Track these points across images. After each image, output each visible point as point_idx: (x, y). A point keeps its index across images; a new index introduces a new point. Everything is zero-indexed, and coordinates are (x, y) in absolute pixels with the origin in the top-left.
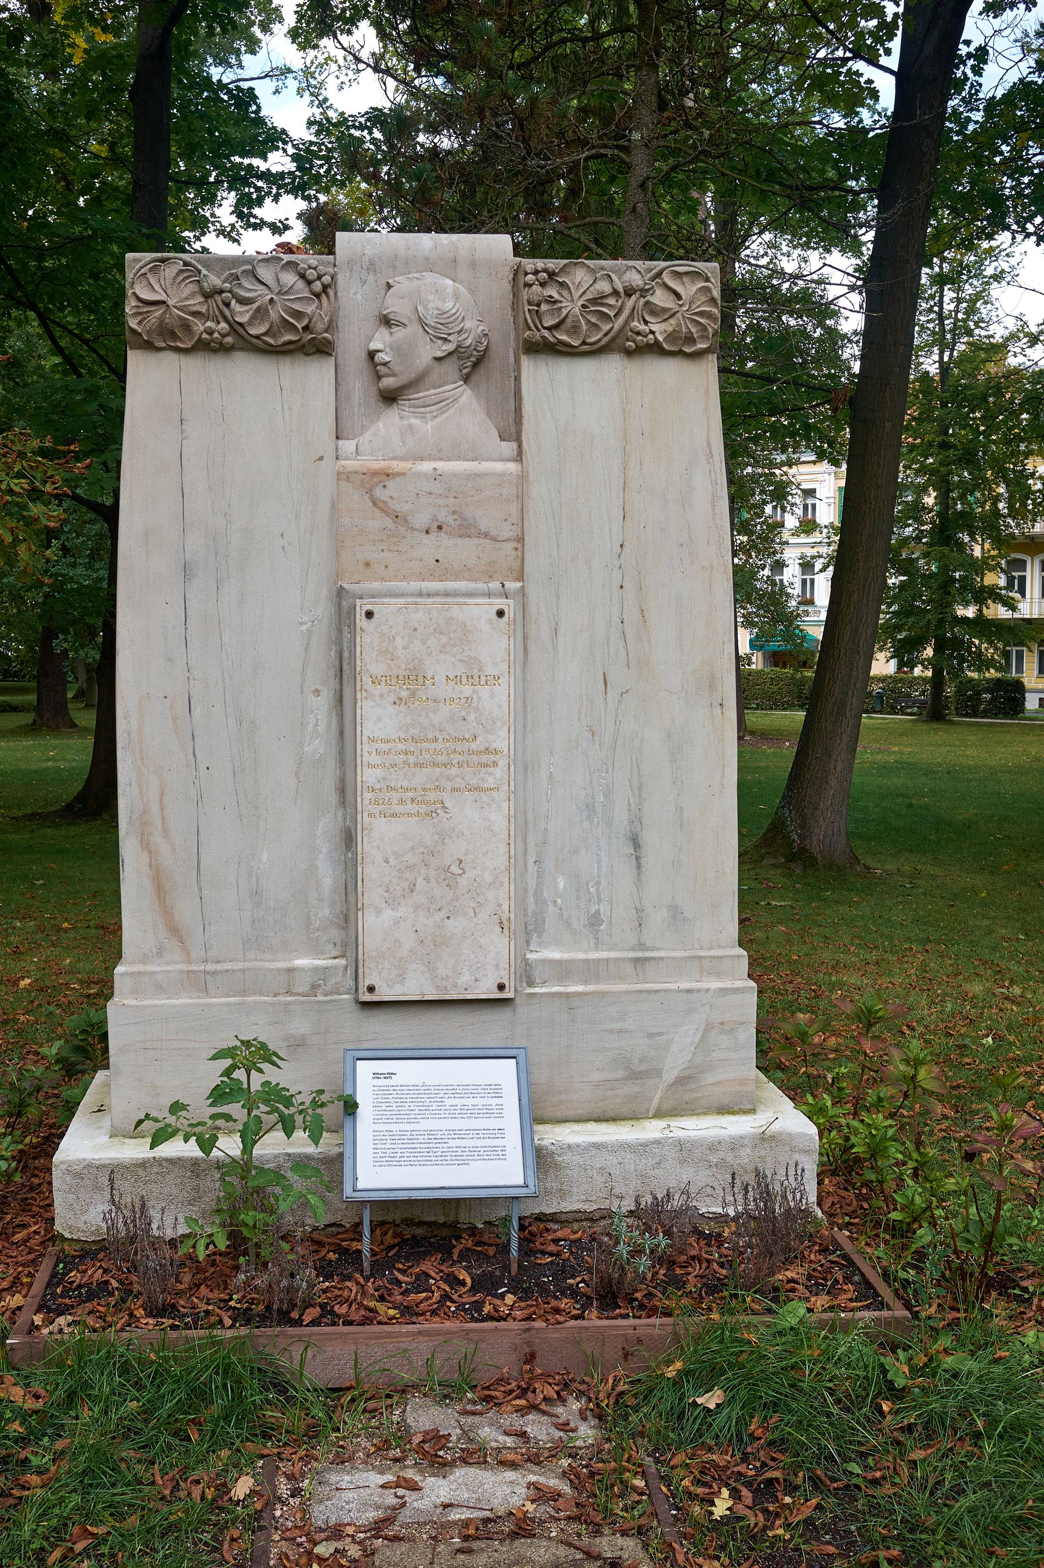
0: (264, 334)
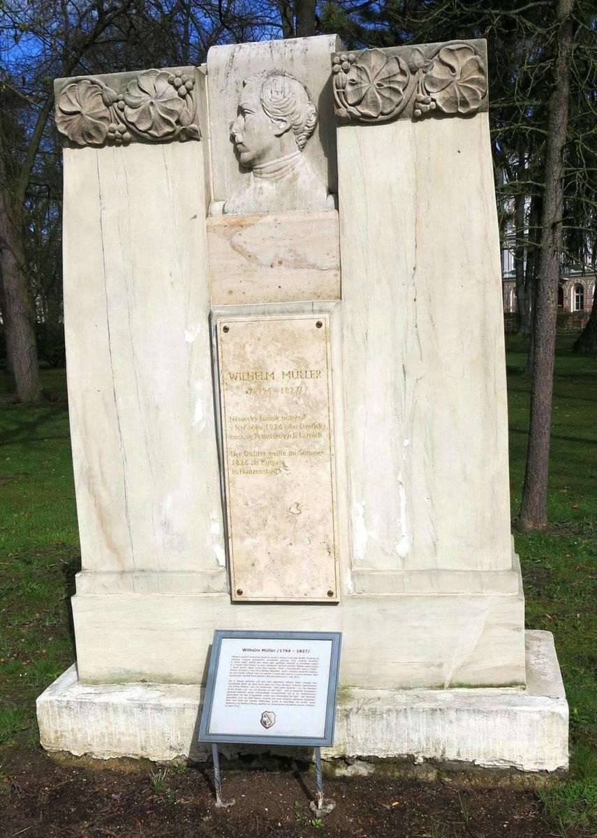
0: (150, 129)
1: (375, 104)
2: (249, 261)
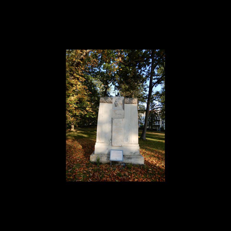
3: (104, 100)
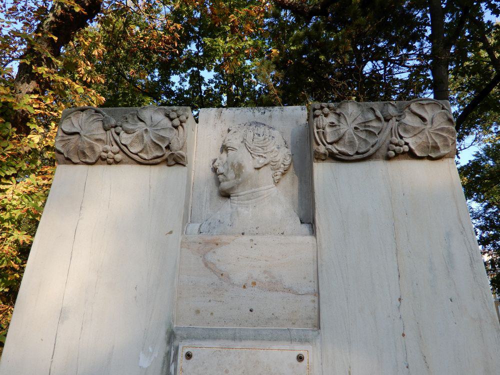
0: (141, 152)
1: (351, 143)
2: (220, 279)
3: (100, 133)
